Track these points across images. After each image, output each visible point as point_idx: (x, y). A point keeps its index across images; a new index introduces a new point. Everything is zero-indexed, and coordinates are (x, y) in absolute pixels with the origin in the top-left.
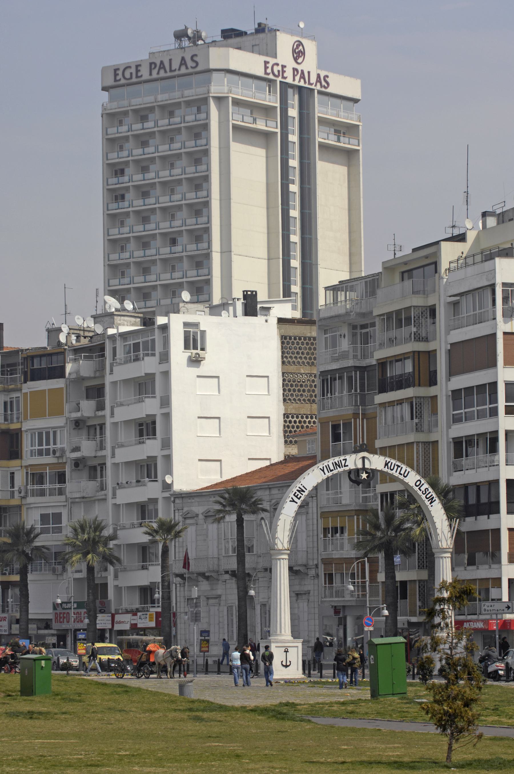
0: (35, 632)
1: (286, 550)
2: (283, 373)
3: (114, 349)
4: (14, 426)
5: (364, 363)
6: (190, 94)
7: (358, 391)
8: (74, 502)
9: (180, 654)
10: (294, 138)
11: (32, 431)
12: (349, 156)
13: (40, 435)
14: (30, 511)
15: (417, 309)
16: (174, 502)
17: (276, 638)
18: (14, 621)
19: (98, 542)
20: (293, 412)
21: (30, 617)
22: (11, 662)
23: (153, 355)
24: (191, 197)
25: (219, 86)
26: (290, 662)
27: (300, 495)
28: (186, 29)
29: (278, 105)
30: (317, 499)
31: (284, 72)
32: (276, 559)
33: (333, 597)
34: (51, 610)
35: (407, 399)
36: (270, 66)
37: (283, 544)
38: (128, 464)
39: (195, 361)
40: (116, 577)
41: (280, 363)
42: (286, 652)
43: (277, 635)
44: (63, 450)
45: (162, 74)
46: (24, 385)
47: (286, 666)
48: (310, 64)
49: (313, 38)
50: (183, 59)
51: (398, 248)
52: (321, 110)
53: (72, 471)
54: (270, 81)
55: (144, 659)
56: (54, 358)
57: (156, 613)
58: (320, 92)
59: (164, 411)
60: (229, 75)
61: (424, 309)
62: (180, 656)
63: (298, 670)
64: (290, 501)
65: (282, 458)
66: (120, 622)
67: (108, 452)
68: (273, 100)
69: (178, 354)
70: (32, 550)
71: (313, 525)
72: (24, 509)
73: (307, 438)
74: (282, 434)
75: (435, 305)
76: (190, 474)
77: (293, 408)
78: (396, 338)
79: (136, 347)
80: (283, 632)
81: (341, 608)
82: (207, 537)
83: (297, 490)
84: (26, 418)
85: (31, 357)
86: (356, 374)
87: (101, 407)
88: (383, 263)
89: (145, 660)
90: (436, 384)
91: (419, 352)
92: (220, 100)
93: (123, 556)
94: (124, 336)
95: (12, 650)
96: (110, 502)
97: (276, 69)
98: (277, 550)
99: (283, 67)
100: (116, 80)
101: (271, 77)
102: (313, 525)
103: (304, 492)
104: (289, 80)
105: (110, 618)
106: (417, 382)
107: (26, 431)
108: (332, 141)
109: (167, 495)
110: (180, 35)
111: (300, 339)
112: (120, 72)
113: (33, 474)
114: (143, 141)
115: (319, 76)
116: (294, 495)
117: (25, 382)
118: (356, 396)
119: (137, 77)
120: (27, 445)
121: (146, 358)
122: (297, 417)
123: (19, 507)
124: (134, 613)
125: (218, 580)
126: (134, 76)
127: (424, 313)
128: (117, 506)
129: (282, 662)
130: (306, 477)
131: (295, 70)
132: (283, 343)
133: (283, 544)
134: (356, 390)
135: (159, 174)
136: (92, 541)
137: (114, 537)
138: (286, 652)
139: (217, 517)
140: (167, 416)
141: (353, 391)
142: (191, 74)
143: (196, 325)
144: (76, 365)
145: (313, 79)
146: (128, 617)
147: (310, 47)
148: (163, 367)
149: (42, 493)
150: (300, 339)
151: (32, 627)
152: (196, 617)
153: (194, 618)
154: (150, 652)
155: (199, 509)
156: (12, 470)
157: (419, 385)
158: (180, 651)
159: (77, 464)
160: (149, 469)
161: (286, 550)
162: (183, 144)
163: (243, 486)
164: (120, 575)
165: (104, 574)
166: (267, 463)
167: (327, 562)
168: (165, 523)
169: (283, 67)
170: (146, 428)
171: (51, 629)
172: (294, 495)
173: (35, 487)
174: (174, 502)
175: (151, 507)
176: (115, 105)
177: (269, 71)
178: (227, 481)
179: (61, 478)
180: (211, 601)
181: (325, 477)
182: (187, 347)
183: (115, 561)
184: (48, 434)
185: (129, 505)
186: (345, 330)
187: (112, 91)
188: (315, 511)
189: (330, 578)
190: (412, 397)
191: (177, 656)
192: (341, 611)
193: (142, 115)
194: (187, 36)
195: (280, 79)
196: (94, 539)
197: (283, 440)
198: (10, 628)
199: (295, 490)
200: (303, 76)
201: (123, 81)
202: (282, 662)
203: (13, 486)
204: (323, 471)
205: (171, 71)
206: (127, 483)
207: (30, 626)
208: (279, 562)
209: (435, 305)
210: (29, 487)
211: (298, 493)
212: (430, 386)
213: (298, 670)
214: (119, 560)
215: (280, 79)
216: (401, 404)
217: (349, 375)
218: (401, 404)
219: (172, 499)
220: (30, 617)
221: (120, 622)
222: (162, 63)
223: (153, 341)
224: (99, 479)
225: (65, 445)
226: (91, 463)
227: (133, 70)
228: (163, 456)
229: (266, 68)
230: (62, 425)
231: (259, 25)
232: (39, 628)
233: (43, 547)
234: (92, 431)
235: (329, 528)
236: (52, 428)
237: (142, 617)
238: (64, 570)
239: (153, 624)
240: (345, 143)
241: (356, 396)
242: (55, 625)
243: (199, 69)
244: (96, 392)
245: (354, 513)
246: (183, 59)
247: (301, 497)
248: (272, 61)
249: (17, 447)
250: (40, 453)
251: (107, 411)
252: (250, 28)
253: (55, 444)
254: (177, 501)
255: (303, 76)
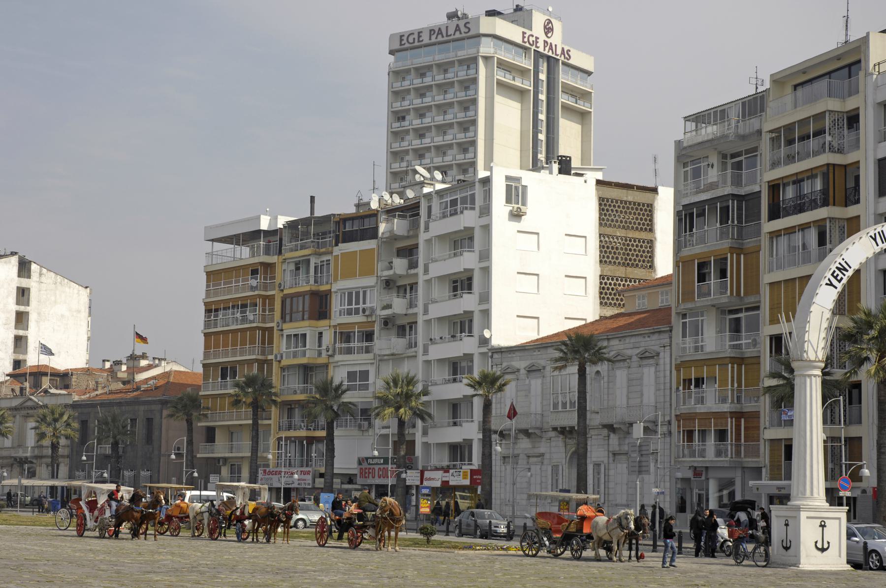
0: (339, 487)
1: (819, 361)
2: (600, 235)
3: (430, 208)
4: (323, 288)
5: (742, 191)
6: (462, 54)
7: (736, 222)
8: (381, 359)
9: (632, 523)
10: (543, 97)
11: (342, 291)
12: (583, 116)
13: (350, 294)
14: (337, 369)
15: (832, 114)
16: (492, 357)
17: (805, 503)
18: (318, 475)
19: (411, 396)
20: (609, 274)
21: (335, 471)
22: (358, 525)
23: (473, 209)
24: (461, 137)
25: (487, 48)
26: (828, 543)
27: (841, 275)
28: (457, 11)
29: (532, 68)
30: (671, 349)
31: (537, 42)
32: (805, 376)
33: (695, 456)
34: (355, 465)
35: (814, 222)
36: (527, 36)
37: (816, 353)
38: (440, 319)
39: (516, 216)
40: (425, 433)
41: (597, 224)
42: (823, 526)
43: (805, 498)
44: (373, 310)
45: (440, 38)
46: (336, 249)
47: (823, 550)
48: (556, 39)
49: (559, 19)
50: (458, 25)
51: (759, 83)
52: (564, 77)
53: (382, 329)
54: (526, 49)
55: (573, 529)
56: (367, 221)
57: (471, 470)
58: (564, 64)
59: (483, 265)
60: (495, 40)
61: (841, 115)
62: (632, 526)
63: (840, 556)
64: (827, 284)
65: (597, 318)
66: (430, 479)
67: (420, 309)
68: (527, 64)
69: (500, 208)
70: (339, 406)
71: (665, 377)
72: (331, 368)
73: (637, 293)
74: (598, 295)
75: (858, 108)
76: (507, 329)
77: (610, 270)
78: (798, 153)
79: (454, 203)
80: (815, 495)
81: (704, 469)
82: (530, 392)
83: (837, 268)
84: (336, 280)
85: (344, 220)
86: (733, 203)
87: (413, 265)
88: (771, 75)
89: (574, 530)
90: (858, 201)
91: (834, 165)
92: (486, 58)
93: (433, 410)
94: (440, 193)
95: (359, 507)
96: (421, 358)
97: (531, 39)
98: (806, 360)
99: (537, 38)
100: (401, 45)
101: (527, 45)
102: (665, 377)
103: (847, 271)
104: (541, 50)
105: (419, 475)
106: (831, 200)
107: (336, 292)
108: (571, 102)
109: (484, 350)
110: (452, 16)
111: (617, 202)
112: (405, 38)
113: (341, 333)
114: (421, 92)
115: (563, 49)
116: (832, 275)
117: (337, 245)
118: (733, 228)
119: (419, 41)
120: (336, 305)
121: (465, 212)
122: (612, 279)
123: (326, 366)
124: (446, 470)
125: (541, 437)
126: (416, 40)
127: (841, 120)
128: (428, 362)
129: (816, 542)
130: (850, 247)
131: (545, 42)
132: (600, 205)
133: (816, 353)
134: (733, 222)
135: (433, 119)
136: (403, 396)
137: (425, 392)
138: (823, 526)
139: (562, 363)
140: (487, 271)
141: (730, 222)
142: (463, 39)
143: (518, 179)
144: (389, 225)
145: (559, 52)
146: (439, 475)
147: (557, 25)
148: (484, 221)
149: (349, 351)
150: (617, 202)
151: (337, 481)
152: (640, 467)
153: (637, 469)
154: (583, 518)
155: (521, 364)
156: (320, 330)
157: (834, 205)
158: (633, 518)
159: (387, 322)
160: (462, 324)
161: (819, 361)
162: (455, 95)
163: (586, 333)
164: (430, 431)
165: (411, 431)
166: (583, 323)
167: (688, 418)
168: (494, 374)
169: (537, 38)
170: (461, 283)
171: (356, 484)
172: (832, 275)
173: (343, 345)
174: (492, 357)
175: (464, 364)
176: (400, 64)
177: (526, 40)
178: (542, 339)
179: (369, 336)
180: (532, 460)
181: (878, 249)
182: (508, 200)
183: (426, 417)
184: (358, 294)
185: (441, 361)
186: (714, 159)
187: (397, 54)
188: (668, 360)
189: (690, 435)
190: (825, 219)
191: (628, 528)
192: (704, 473)
193: (421, 72)
194: (458, 17)
195: (534, 48)
196: (407, 393)
197: (598, 301)
198: (314, 482)
199: (833, 268)
200: (551, 48)
201: (407, 45)
202: (816, 542)
203: (320, 346)
204: (875, 239)
205: (447, 36)
206: (441, 338)
207: (335, 480)
208: (808, 380)
209: (858, 108)
210: (337, 345)
211: (837, 272)
212: (846, 206)
213: (840, 556)
214: (430, 415)
215: (534, 48)
216: (803, 230)
217: (725, 204)
218: (803, 230)
219: (490, 354)
220: (335, 471)
221: (430, 479)
222: (440, 29)
223: (473, 196)
224: (408, 337)
225: (375, 305)
226: (400, 322)
227: (416, 36)
228: (481, 311)
229: (524, 37)
230: (373, 284)
231: (517, 6)
232: (342, 483)
233: (350, 403)
234: (402, 291)
235: (703, 379)
236: (363, 288)
237: (455, 474)
238: (370, 425)
239: (467, 482)
240: (581, 106)
241: (733, 228)
242: (360, 480)
243: (470, 34)
244: (409, 252)
245: (727, 361)
246: (458, 25)
247: (842, 279)
248: (528, 33)
249: (326, 308)
250: (349, 312)
251: (420, 269)
252: (508, 9)
253: (364, 303)
254: (496, 356)
255: (551, 48)
